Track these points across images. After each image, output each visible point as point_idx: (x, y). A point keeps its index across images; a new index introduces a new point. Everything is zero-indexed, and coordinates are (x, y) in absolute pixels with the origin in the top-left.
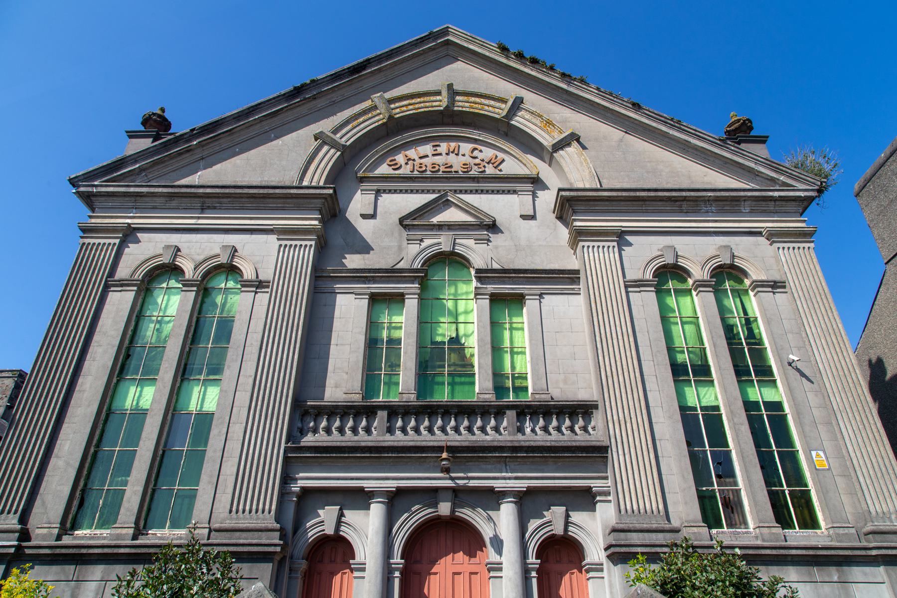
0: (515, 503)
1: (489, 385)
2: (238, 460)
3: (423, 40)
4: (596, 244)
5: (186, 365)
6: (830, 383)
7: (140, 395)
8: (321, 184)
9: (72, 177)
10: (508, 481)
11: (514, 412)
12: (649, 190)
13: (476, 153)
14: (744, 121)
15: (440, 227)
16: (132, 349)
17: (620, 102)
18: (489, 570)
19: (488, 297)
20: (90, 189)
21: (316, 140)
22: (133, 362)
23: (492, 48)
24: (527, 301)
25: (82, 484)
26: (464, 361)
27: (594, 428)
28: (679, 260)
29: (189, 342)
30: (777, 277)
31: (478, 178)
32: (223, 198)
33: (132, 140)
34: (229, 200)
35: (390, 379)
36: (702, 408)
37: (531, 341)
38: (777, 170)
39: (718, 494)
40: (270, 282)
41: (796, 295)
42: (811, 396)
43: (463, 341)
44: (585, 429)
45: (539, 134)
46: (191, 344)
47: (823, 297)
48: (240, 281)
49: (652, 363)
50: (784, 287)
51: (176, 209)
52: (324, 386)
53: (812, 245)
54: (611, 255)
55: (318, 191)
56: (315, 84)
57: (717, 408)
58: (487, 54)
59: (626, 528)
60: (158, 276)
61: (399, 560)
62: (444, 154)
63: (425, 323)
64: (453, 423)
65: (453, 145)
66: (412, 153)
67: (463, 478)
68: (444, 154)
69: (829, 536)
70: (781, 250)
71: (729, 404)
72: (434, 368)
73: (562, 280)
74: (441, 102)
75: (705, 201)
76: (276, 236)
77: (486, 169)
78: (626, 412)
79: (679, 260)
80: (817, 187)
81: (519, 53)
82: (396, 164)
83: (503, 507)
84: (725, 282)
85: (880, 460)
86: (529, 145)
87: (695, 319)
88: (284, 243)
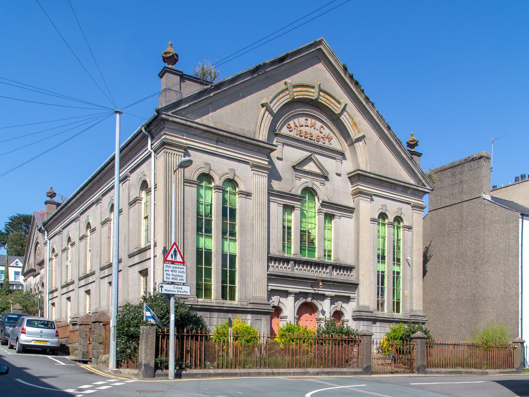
11: (331, 267)
17: (384, 122)
23: (340, 65)
34: (231, 140)
58: (337, 67)
62: (309, 126)
67: (318, 290)
87: (384, 238)
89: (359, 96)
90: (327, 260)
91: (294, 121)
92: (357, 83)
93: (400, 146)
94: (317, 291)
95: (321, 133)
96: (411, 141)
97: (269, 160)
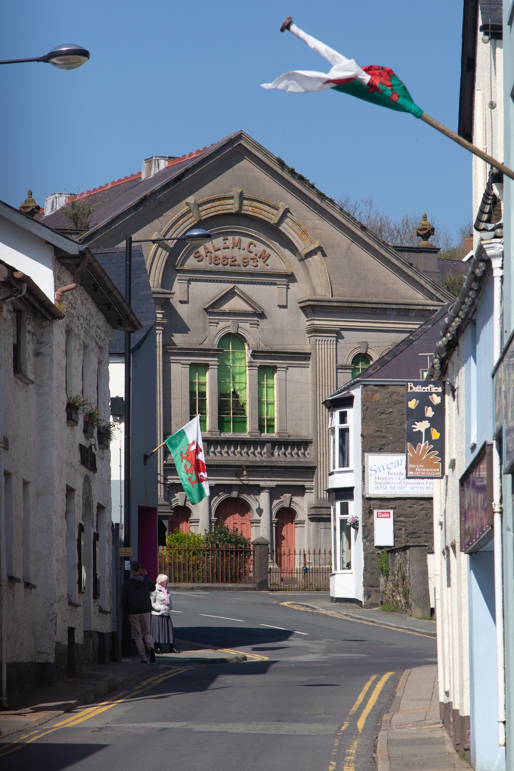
10: (267, 482)
12: (360, 303)
18: (252, 523)
23: (273, 159)
43: (239, 393)
45: (297, 241)
58: (268, 163)
63: (221, 383)
90: (266, 433)
91: (204, 246)
92: (301, 179)
93: (387, 250)
95: (251, 252)
97: (164, 312)
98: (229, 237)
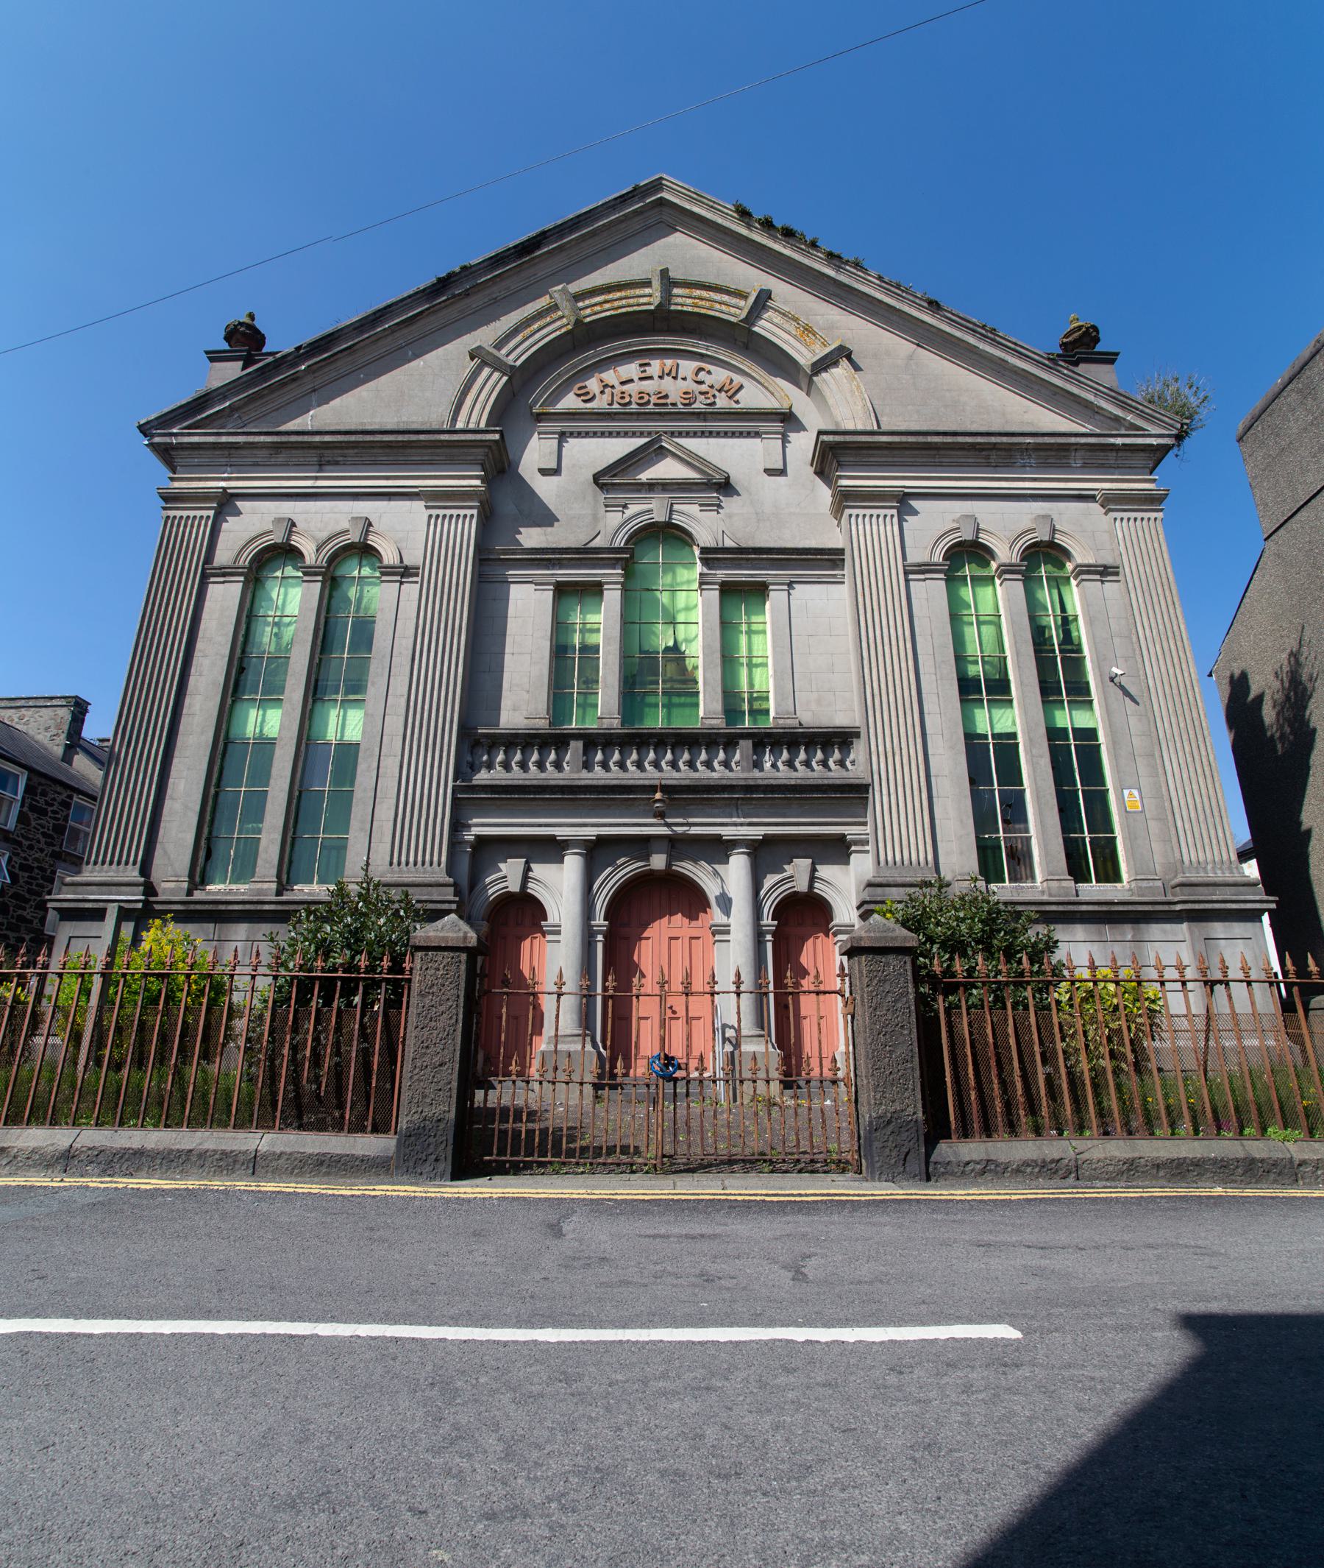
0: (748, 854)
1: (718, 706)
2: (395, 801)
3: (624, 200)
4: (868, 512)
5: (317, 681)
6: (1159, 704)
7: (263, 721)
8: (482, 425)
9: (142, 422)
10: (739, 828)
13: (702, 376)
14: (1087, 328)
15: (652, 486)
16: (246, 659)
17: (911, 298)
19: (717, 587)
20: (167, 440)
21: (472, 359)
22: (249, 677)
24: (771, 593)
25: (206, 830)
26: (684, 675)
27: (853, 762)
28: (981, 535)
29: (318, 650)
30: (1108, 560)
31: (705, 413)
32: (347, 448)
33: (215, 364)
34: (356, 451)
35: (586, 699)
36: (994, 736)
37: (774, 648)
38: (1124, 406)
39: (1002, 843)
40: (418, 568)
41: (1131, 585)
42: (1133, 721)
43: (683, 648)
44: (841, 763)
45: (793, 347)
46: (321, 654)
47: (1166, 587)
48: (379, 567)
49: (934, 677)
50: (1117, 574)
51: (285, 466)
52: (498, 709)
53: (1160, 515)
54: (889, 528)
55: (478, 437)
56: (467, 273)
57: (1014, 735)
58: (720, 221)
59: (885, 882)
60: (270, 560)
61: (602, 922)
62: (656, 377)
63: (630, 623)
64: (669, 756)
65: (669, 363)
66: (610, 376)
67: (682, 825)
68: (656, 377)
69: (1130, 890)
70: (1118, 522)
71: (1029, 730)
72: (643, 684)
73: (820, 563)
74: (650, 298)
75: (1021, 451)
76: (423, 503)
77: (717, 400)
78: (896, 740)
79: (981, 535)
80: (1175, 432)
81: (766, 219)
82: (587, 393)
83: (732, 859)
84: (1040, 567)
85: (1205, 799)
86: (778, 362)
87: (995, 620)
88: (434, 512)
89: (806, 261)
92: (788, 234)
94: (679, 829)
96: (1066, 336)
98: (651, 362)
